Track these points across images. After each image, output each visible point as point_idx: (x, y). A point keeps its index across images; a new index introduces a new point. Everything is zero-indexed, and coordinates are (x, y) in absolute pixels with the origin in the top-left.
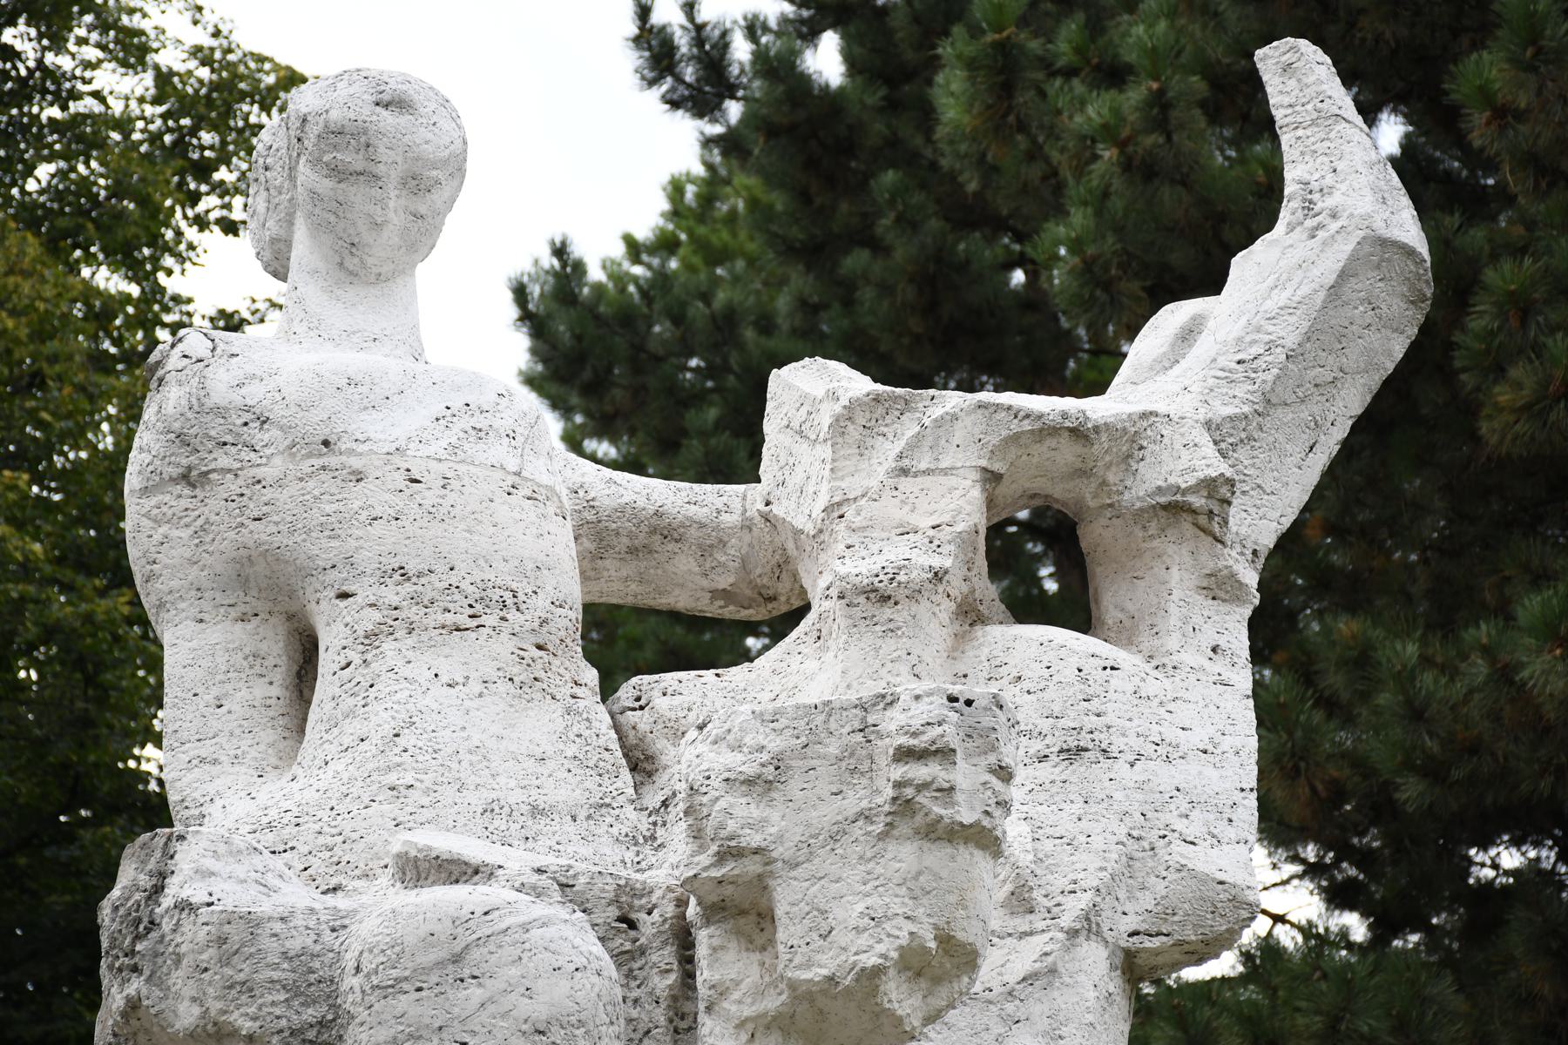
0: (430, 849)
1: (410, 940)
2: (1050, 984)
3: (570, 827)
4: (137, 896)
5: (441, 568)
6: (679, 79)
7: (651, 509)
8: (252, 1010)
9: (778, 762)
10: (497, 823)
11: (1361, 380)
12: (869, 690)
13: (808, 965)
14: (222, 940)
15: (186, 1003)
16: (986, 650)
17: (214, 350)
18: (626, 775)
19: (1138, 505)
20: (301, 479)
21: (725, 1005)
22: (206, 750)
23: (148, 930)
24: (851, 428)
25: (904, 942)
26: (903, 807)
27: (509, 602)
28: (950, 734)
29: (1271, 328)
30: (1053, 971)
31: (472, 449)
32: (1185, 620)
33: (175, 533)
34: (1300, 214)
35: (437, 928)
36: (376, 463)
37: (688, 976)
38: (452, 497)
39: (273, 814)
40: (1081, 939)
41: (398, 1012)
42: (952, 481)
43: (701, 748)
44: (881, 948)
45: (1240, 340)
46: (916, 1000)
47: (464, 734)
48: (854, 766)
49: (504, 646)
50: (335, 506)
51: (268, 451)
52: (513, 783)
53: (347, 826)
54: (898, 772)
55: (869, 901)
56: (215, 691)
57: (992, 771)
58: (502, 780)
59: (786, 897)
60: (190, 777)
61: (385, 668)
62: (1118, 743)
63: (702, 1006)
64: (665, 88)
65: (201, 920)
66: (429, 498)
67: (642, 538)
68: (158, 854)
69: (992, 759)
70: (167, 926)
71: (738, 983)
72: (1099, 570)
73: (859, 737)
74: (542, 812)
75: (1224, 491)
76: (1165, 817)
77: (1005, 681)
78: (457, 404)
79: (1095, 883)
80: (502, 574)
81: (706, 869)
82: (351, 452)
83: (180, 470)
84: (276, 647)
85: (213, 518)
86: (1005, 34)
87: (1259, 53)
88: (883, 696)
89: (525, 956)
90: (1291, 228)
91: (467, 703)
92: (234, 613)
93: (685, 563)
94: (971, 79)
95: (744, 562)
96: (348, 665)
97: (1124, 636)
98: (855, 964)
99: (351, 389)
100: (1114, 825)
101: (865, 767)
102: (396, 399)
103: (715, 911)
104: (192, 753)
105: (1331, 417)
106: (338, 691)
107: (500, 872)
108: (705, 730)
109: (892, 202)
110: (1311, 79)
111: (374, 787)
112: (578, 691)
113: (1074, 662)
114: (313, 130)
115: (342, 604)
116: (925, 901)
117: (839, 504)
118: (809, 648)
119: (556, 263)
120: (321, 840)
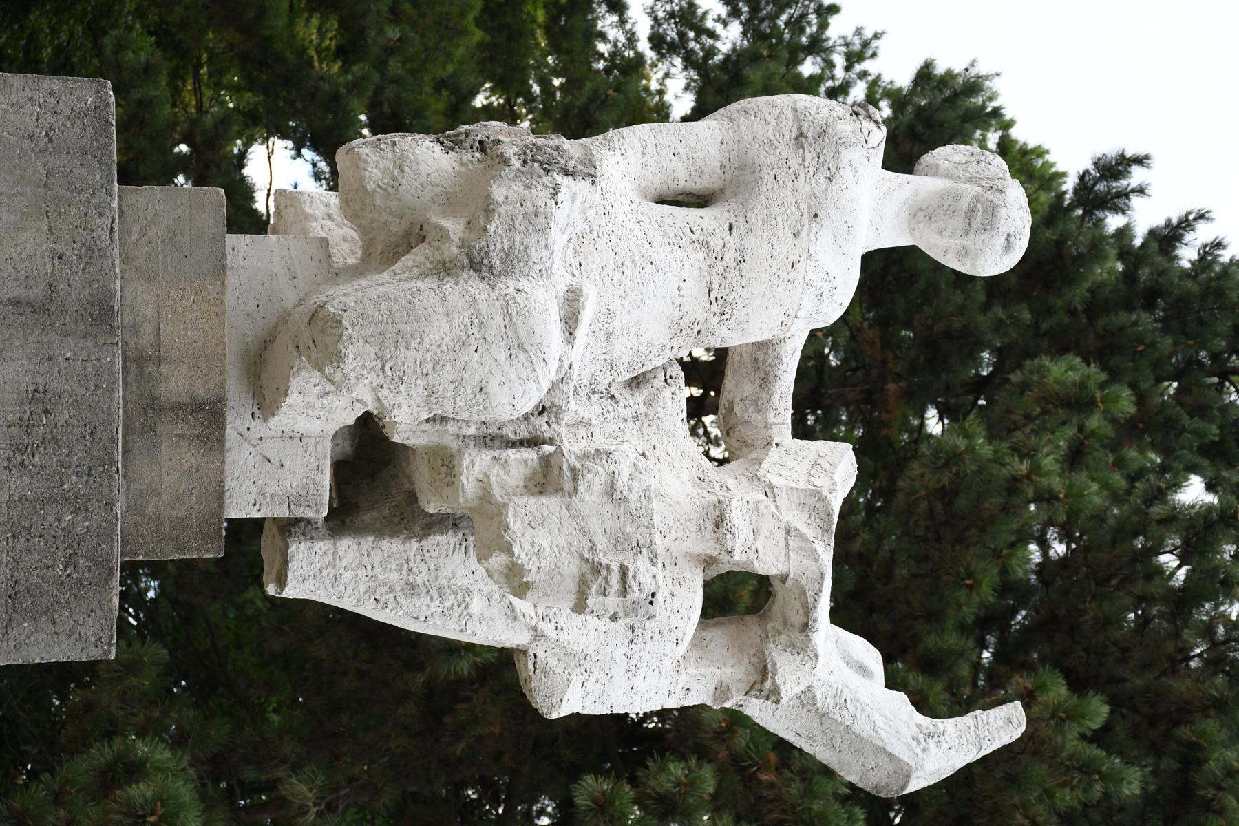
0: (584, 309)
1: (531, 321)
2: (509, 617)
3: (600, 352)
4: (563, 162)
5: (744, 282)
6: (1096, 182)
7: (778, 373)
8: (500, 231)
9: (623, 500)
10: (603, 317)
11: (835, 760)
13: (516, 515)
14: (537, 214)
15: (505, 193)
16: (689, 576)
17: (873, 148)
18: (628, 376)
19: (767, 653)
20: (796, 202)
21: (497, 467)
23: (544, 169)
24: (815, 500)
25: (526, 567)
26: (597, 569)
27: (724, 317)
28: (635, 595)
29: (863, 717)
30: (515, 619)
31: (811, 293)
32: (704, 676)
34: (926, 731)
35: (537, 335)
36: (803, 246)
37: (512, 444)
38: (783, 285)
39: (611, 199)
40: (532, 633)
41: (494, 316)
42: (782, 558)
43: (632, 456)
44: (523, 555)
45: (858, 700)
46: (496, 566)
47: (652, 296)
48: (620, 542)
49: (700, 315)
50: (780, 222)
51: (813, 182)
52: (624, 322)
53: (603, 240)
54: (615, 567)
55: (548, 549)
56: (682, 152)
57: (614, 614)
58: (627, 316)
59: (551, 502)
60: (636, 141)
61: (689, 254)
62: (636, 647)
63: (496, 453)
64: (1093, 172)
65: (548, 201)
66: (783, 274)
67: (762, 367)
68: (585, 170)
69: (621, 614)
70: (547, 180)
71: (508, 473)
72: (734, 626)
73: (635, 543)
74: (608, 338)
75: (773, 698)
76: (596, 671)
77: (672, 588)
78: (836, 283)
79: (561, 640)
80: (739, 313)
81: (567, 461)
82: (810, 230)
83: (805, 132)
84: (704, 183)
85: (778, 151)
86: (1100, 404)
87: (1018, 703)
88: (656, 557)
89: (521, 381)
91: (669, 297)
92: (725, 161)
93: (748, 389)
94: (1074, 384)
96: (692, 232)
97: (697, 643)
98: (515, 541)
99: (846, 228)
100: (592, 648)
102: (840, 251)
103: (546, 461)
104: (649, 143)
105: (815, 744)
106: (678, 226)
107: (570, 347)
108: (641, 458)
109: (1011, 317)
110: (1002, 734)
111: (623, 254)
112: (675, 349)
113: (681, 625)
114: (995, 197)
115: (726, 228)
116: (547, 577)
117: (773, 492)
118: (695, 473)
119: (989, 109)
120: (596, 227)
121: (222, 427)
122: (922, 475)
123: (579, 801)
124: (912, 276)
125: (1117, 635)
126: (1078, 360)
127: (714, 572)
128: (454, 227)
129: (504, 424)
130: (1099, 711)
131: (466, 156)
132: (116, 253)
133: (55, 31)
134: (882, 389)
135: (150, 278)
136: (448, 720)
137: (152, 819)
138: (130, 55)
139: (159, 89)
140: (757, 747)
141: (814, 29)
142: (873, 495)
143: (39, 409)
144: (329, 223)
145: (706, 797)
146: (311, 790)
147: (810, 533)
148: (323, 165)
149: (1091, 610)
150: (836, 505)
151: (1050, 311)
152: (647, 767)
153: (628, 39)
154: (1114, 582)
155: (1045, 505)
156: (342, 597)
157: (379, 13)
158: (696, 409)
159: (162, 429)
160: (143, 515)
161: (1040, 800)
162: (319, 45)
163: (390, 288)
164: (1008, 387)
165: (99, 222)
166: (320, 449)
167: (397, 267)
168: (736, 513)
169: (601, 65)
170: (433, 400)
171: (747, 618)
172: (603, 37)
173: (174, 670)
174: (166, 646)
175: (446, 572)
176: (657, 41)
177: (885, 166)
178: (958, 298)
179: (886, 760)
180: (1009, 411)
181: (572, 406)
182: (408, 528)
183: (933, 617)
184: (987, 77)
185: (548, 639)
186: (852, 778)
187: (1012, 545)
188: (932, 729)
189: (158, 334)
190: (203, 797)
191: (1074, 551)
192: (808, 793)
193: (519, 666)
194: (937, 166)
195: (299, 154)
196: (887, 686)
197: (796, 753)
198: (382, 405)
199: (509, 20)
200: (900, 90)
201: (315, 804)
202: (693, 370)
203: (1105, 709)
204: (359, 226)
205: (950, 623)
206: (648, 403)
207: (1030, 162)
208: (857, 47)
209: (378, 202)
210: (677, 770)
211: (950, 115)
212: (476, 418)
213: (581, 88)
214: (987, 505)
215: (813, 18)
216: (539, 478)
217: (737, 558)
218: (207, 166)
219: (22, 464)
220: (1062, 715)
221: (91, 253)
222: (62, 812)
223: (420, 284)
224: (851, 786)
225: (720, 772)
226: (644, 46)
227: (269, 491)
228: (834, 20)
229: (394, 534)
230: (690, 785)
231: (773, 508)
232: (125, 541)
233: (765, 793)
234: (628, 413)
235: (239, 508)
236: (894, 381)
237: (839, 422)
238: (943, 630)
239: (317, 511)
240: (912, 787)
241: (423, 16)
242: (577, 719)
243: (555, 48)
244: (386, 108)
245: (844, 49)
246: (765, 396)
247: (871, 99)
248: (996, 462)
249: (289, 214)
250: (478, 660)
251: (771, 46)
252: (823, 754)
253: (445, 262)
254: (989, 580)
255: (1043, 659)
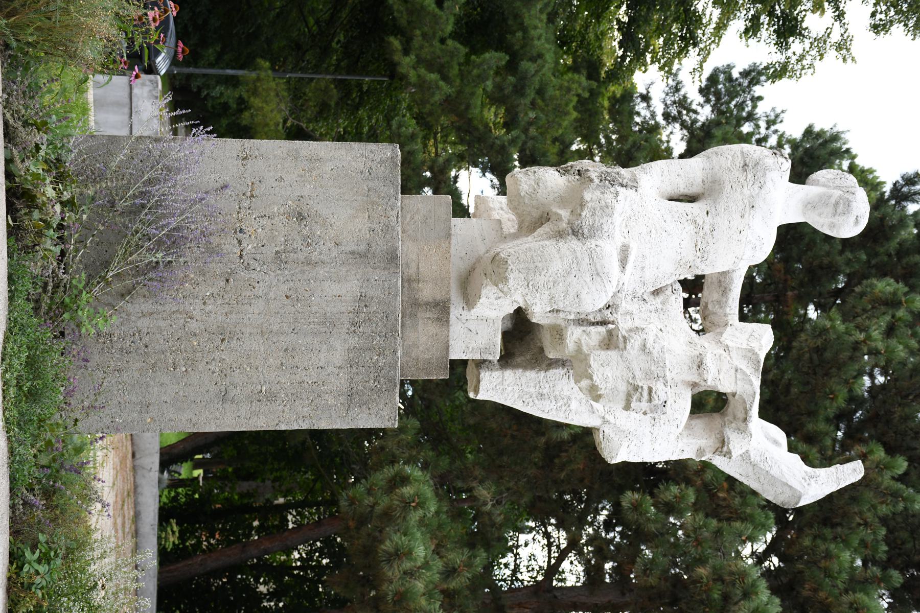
4: (621, 181)
6: (903, 186)
7: (732, 288)
8: (588, 215)
9: (650, 353)
12: (669, 378)
13: (594, 360)
22: (666, 173)
26: (636, 388)
28: (656, 402)
30: (593, 412)
32: (691, 444)
33: (729, 162)
37: (593, 324)
42: (733, 384)
44: (598, 381)
45: (773, 458)
48: (648, 374)
49: (691, 258)
51: (752, 189)
54: (646, 388)
56: (682, 174)
59: (613, 354)
63: (585, 328)
64: (901, 182)
67: (723, 285)
69: (649, 412)
70: (612, 189)
71: (590, 339)
73: (656, 375)
75: (728, 456)
78: (763, 241)
82: (750, 214)
87: (860, 461)
90: (806, 472)
92: (705, 179)
93: (716, 296)
94: (890, 293)
95: (715, 313)
97: (688, 427)
101: (648, 377)
103: (610, 333)
109: (855, 257)
114: (850, 197)
118: (688, 339)
119: (844, 150)
120: (637, 213)
121: (448, 314)
122: (806, 340)
123: (624, 504)
124: (801, 236)
125: (913, 425)
126: (892, 280)
127: (697, 390)
128: (564, 213)
129: (589, 314)
130: (902, 465)
131: (571, 178)
132: (399, 228)
133: (370, 118)
134: (785, 295)
135: (415, 240)
136: (557, 461)
137: (413, 504)
138: (404, 129)
139: (418, 146)
140: (717, 479)
141: (750, 108)
142: (779, 349)
143: (362, 304)
144: (501, 212)
145: (690, 504)
146: (489, 493)
147: (748, 371)
148: (496, 181)
149: (898, 412)
150: (762, 358)
151: (876, 254)
152: (659, 488)
153: (652, 115)
154: (911, 397)
155: (873, 356)
156: (506, 400)
157: (525, 105)
158: (687, 303)
159: (419, 315)
160: (410, 357)
161: (869, 510)
162: (495, 121)
163: (532, 245)
164: (853, 294)
165: (392, 213)
166: (496, 325)
167: (535, 234)
168: (709, 361)
169: (637, 129)
170: (553, 301)
171: (715, 414)
172: (638, 114)
173: (423, 431)
174: (418, 420)
175: (558, 388)
176: (667, 116)
177: (790, 181)
178: (826, 247)
179: (788, 489)
180: (854, 307)
181: (624, 304)
182: (539, 365)
183: (811, 414)
184: (843, 132)
185: (610, 423)
186: (769, 498)
187: (855, 377)
188: (813, 474)
189: (418, 268)
190: (437, 494)
191: (889, 381)
192: (745, 504)
193: (595, 436)
194: (818, 180)
195: (484, 175)
196: (789, 451)
197: (738, 483)
198: (527, 304)
199: (590, 106)
200: (795, 139)
201: (491, 500)
202: (685, 284)
203: (905, 464)
204: (517, 213)
205: (821, 417)
206: (663, 303)
207: (866, 177)
208: (772, 117)
209: (526, 201)
210: (674, 490)
211: (823, 152)
212: (574, 310)
213: (627, 140)
214: (841, 356)
215: (749, 103)
216: (607, 341)
217: (709, 383)
218: (440, 183)
219: (355, 331)
220: (882, 466)
221: (387, 228)
222: (371, 499)
223: (547, 243)
224: (768, 501)
225: (698, 491)
226: (660, 119)
227: (471, 346)
228: (760, 104)
229: (533, 368)
230: (681, 498)
231: (729, 358)
232: (402, 370)
233: (721, 503)
234: (652, 308)
235: (456, 354)
236: (791, 291)
237: (761, 312)
238: (817, 421)
239: (494, 356)
240: (801, 504)
241: (547, 105)
242: (625, 464)
243: (614, 120)
244: (528, 152)
245: (766, 119)
246: (725, 299)
247: (780, 145)
248: (846, 334)
249: (482, 207)
250: (572, 431)
251: (727, 118)
252: (754, 485)
253: (559, 232)
254: (842, 395)
255: (871, 437)
